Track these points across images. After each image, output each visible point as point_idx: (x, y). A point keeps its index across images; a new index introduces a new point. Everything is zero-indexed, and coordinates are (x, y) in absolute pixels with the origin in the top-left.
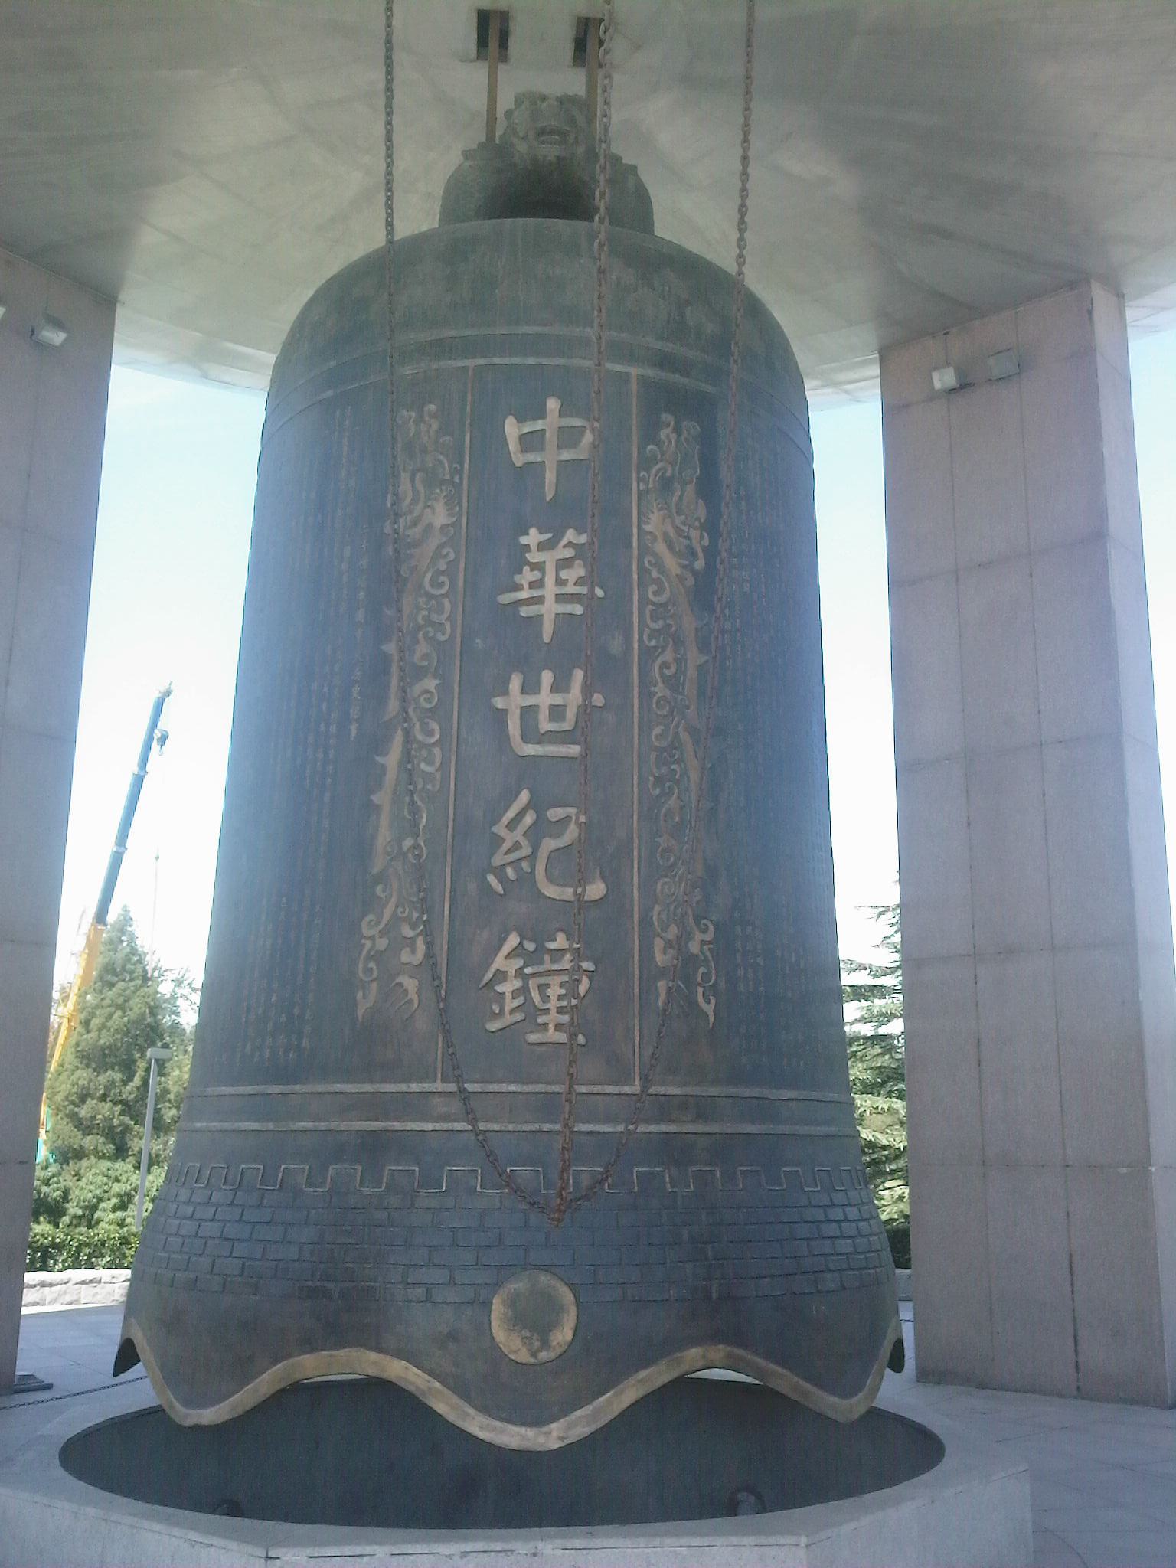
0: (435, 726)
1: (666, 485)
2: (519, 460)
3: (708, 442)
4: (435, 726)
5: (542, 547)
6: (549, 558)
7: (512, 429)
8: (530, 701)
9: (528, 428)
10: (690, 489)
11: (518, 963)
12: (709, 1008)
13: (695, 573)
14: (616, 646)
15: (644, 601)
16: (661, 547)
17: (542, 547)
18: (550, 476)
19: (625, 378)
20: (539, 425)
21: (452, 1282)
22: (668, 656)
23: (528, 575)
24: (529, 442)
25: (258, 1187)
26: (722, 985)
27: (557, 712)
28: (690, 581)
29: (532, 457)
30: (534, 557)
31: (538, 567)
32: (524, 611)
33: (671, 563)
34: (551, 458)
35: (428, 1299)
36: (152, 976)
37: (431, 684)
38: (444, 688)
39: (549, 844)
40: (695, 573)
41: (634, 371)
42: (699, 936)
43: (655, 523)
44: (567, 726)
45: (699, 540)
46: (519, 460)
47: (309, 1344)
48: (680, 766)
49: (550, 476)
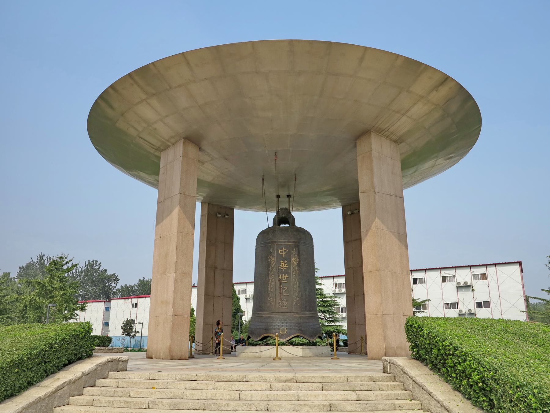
0: (273, 280)
1: (294, 255)
2: (280, 254)
3: (299, 250)
4: (273, 280)
5: (283, 262)
6: (283, 263)
7: (280, 251)
8: (284, 277)
9: (281, 251)
10: (297, 255)
11: (281, 301)
12: (299, 305)
13: (297, 263)
14: (290, 271)
15: (292, 267)
16: (294, 261)
17: (283, 262)
18: (283, 255)
19: (290, 244)
20: (282, 250)
21: (284, 325)
22: (295, 272)
23: (281, 265)
24: (281, 252)
25: (283, 280)
26: (300, 303)
27: (284, 278)
28: (297, 264)
29: (281, 254)
30: (282, 263)
31: (282, 264)
32: (281, 269)
33: (295, 263)
34: (283, 253)
35: (274, 329)
36: (282, 278)
37: (273, 276)
38: (274, 276)
39: (284, 290)
40: (297, 263)
41: (291, 244)
42: (298, 298)
43: (293, 259)
44: (285, 279)
45: (298, 260)
46: (280, 254)
47: (265, 334)
48: (17, 361)
49: (283, 255)
